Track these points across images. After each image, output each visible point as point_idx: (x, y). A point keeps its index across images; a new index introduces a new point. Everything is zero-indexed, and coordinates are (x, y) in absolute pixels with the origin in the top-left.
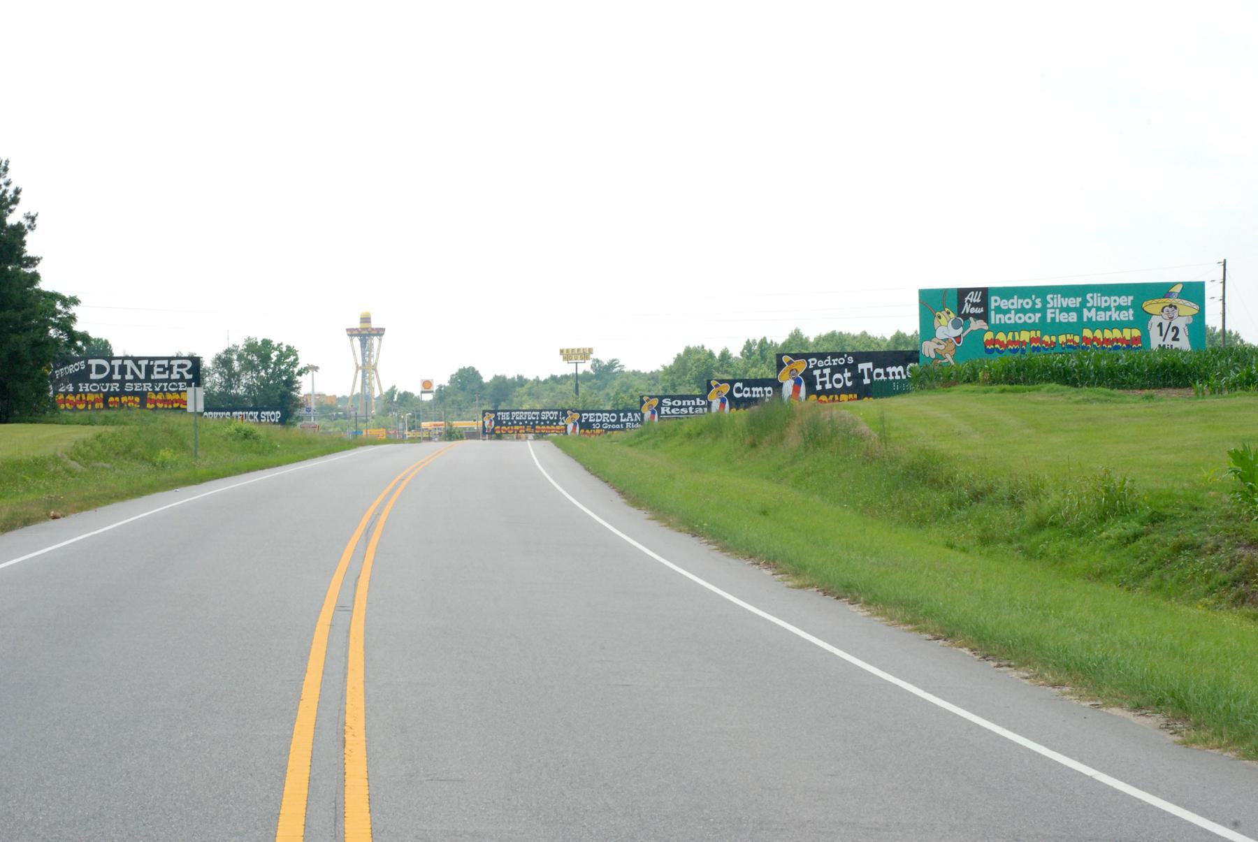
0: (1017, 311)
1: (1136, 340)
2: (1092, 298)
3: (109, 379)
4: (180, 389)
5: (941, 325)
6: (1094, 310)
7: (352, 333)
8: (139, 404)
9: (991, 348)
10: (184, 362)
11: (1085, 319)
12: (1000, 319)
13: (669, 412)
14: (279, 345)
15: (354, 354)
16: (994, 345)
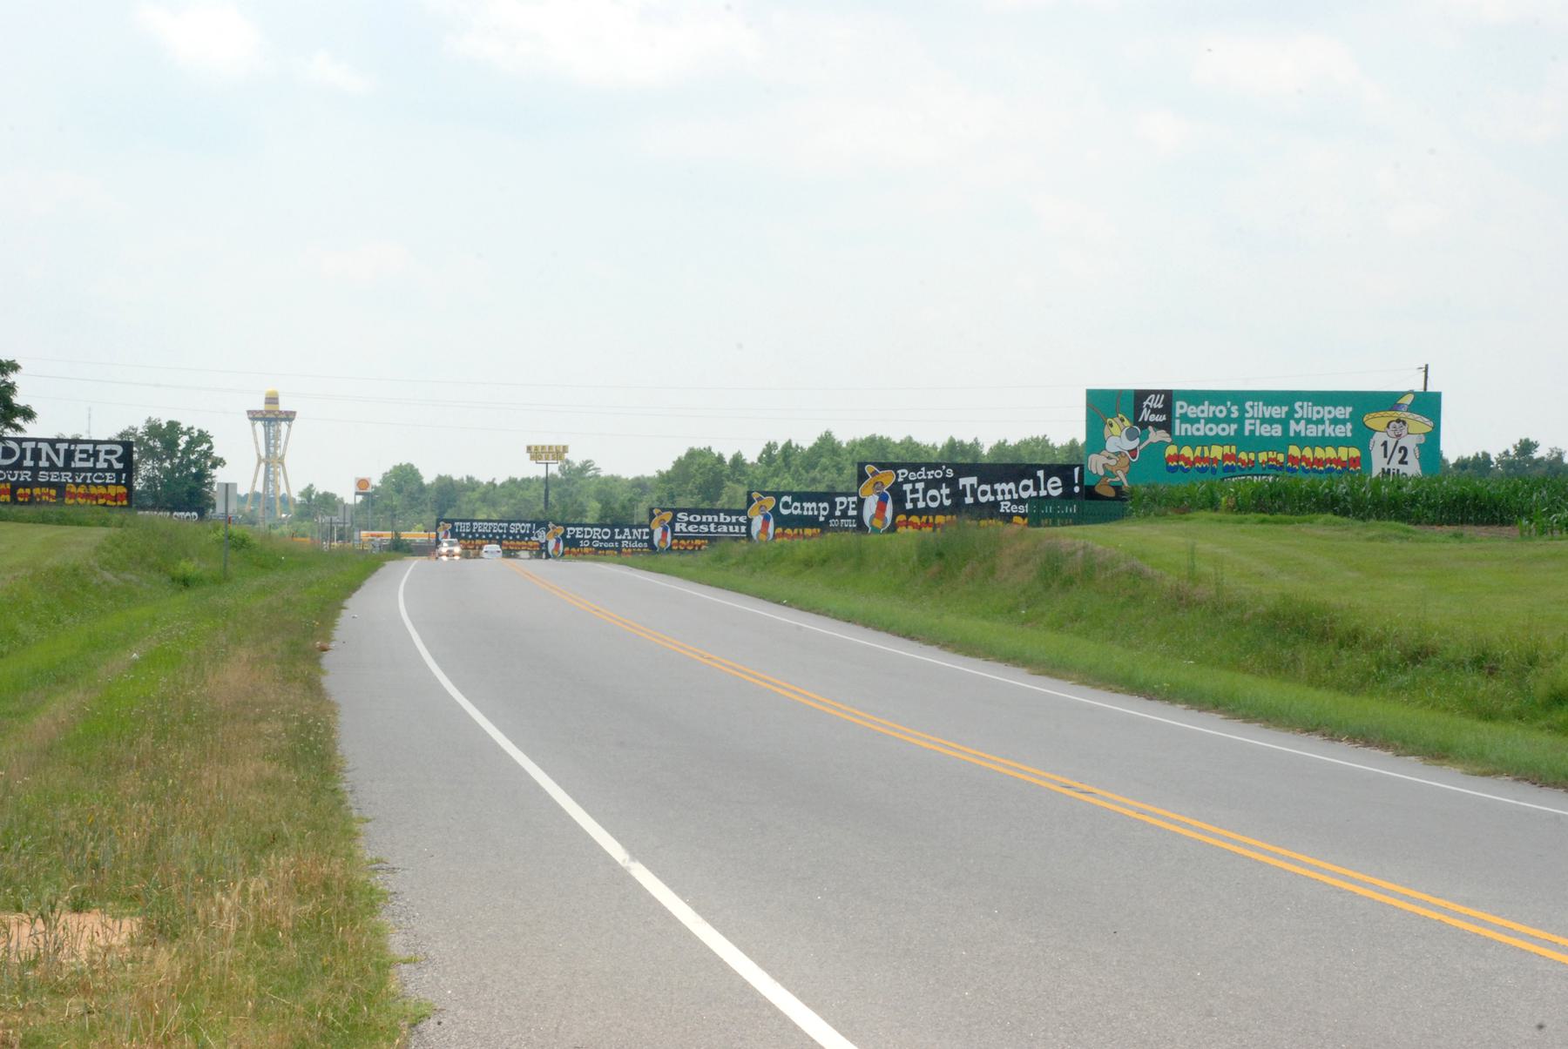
0: (1208, 421)
1: (1354, 461)
2: (1302, 407)
3: (18, 466)
4: (108, 481)
5: (1113, 435)
6: (1303, 422)
7: (254, 416)
8: (55, 498)
9: (1175, 466)
10: (114, 447)
11: (1292, 434)
12: (1186, 429)
13: (685, 530)
14: (189, 429)
15: (256, 443)
16: (1178, 462)
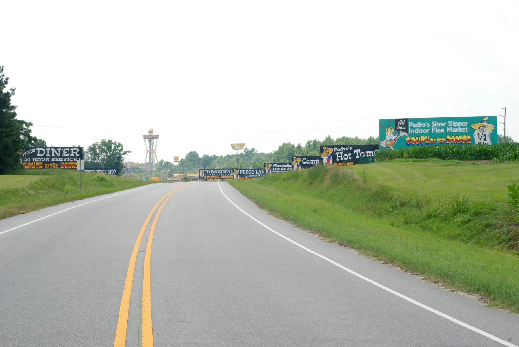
0: (420, 128)
1: (469, 140)
2: (451, 123)
3: (45, 156)
4: (74, 160)
5: (388, 134)
6: (451, 128)
7: (145, 137)
8: (57, 166)
9: (409, 143)
10: (76, 149)
11: (448, 132)
12: (413, 131)
13: (276, 170)
14: (115, 142)
15: (146, 146)
16: (410, 142)
